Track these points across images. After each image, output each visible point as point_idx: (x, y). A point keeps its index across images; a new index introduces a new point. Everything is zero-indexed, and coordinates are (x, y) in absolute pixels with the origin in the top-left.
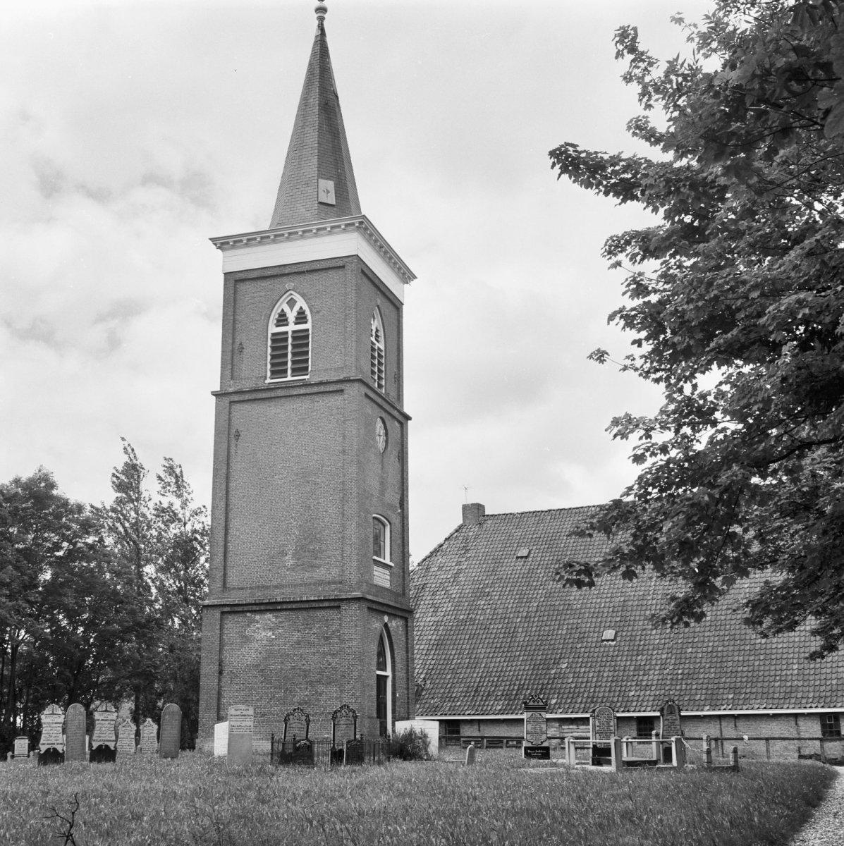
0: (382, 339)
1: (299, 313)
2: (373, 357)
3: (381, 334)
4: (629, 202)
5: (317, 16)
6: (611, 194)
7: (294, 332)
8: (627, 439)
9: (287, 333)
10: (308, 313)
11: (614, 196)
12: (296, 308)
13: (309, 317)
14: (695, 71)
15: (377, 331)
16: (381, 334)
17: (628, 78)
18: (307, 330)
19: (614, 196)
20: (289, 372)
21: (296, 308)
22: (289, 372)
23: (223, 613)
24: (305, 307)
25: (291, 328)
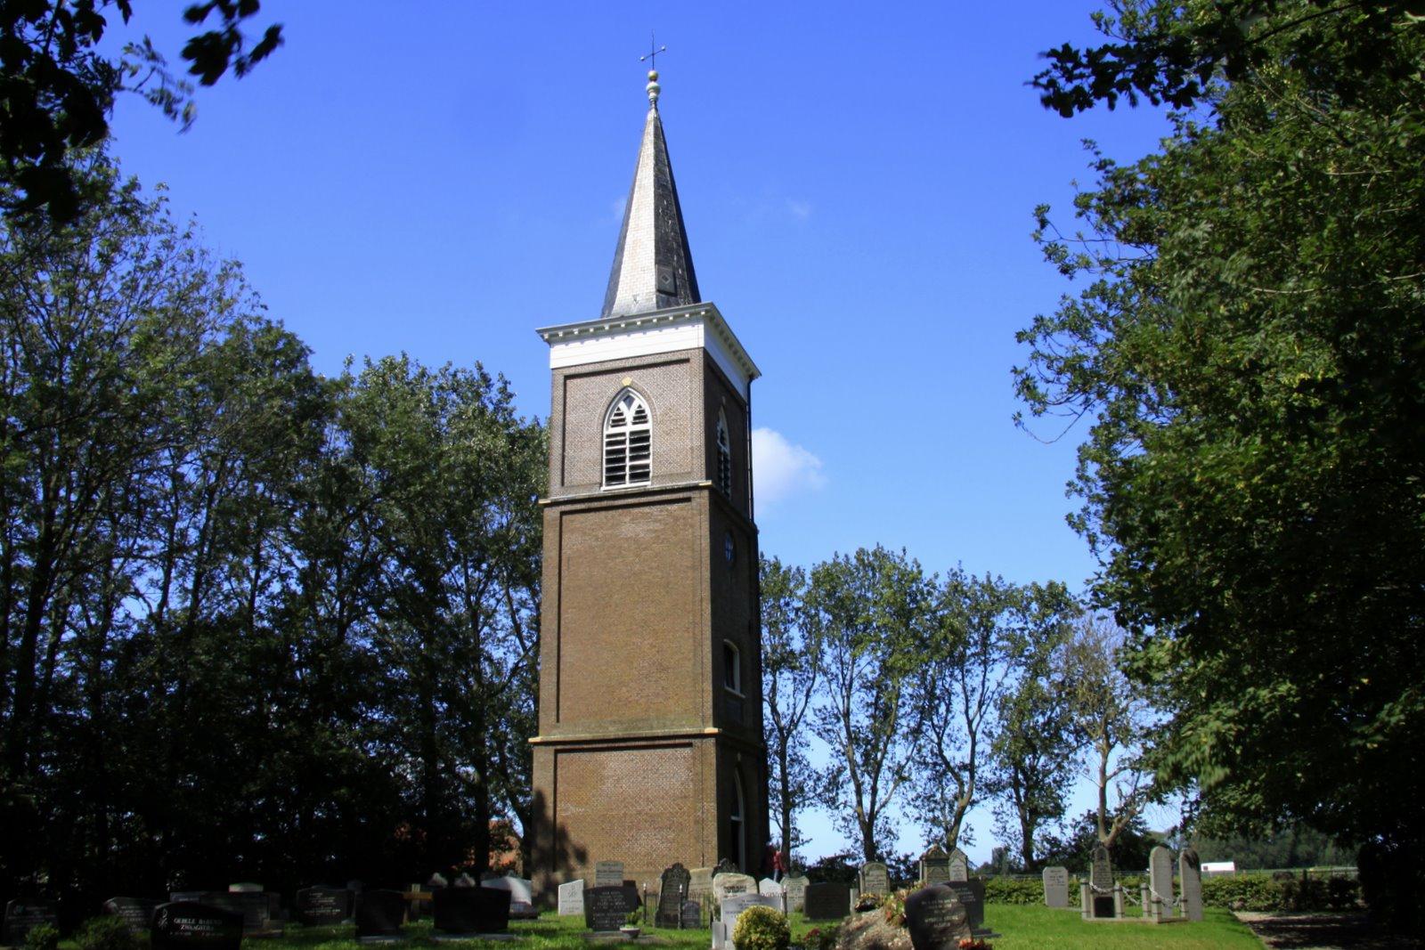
0: (727, 442)
1: (637, 412)
2: (720, 461)
3: (726, 436)
4: (1052, 110)
5: (1095, 101)
6: (1075, 110)
7: (632, 433)
8: (1071, 278)
9: (623, 434)
10: (648, 412)
11: (1081, 109)
12: (634, 407)
13: (650, 418)
14: (119, 605)
15: (722, 432)
16: (726, 436)
17: (511, 396)
18: (647, 431)
19: (1081, 109)
20: (627, 477)
21: (634, 407)
22: (627, 477)
23: (557, 752)
24: (646, 407)
25: (629, 428)
